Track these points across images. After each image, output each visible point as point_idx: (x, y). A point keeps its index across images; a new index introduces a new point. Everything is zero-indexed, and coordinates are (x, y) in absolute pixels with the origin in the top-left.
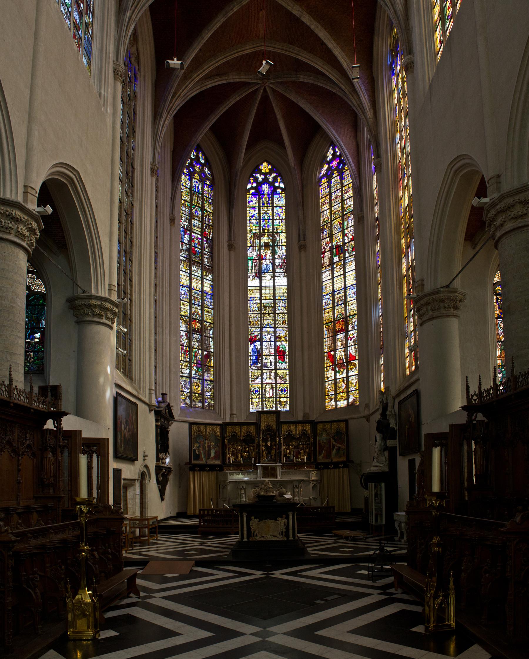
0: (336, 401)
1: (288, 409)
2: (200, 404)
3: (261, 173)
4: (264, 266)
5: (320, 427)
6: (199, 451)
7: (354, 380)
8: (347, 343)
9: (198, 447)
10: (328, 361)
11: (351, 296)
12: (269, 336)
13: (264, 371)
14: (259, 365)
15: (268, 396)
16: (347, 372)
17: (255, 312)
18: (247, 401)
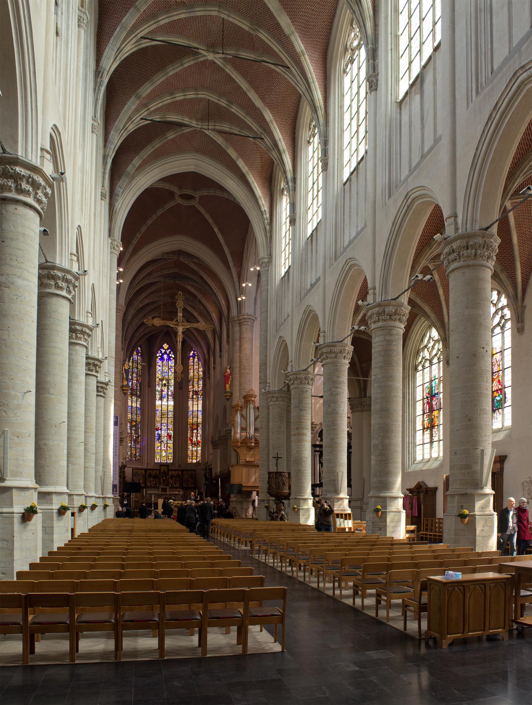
0: (192, 460)
1: (172, 462)
2: (135, 459)
3: (164, 349)
4: (163, 395)
5: (185, 472)
7: (199, 452)
8: (197, 435)
10: (189, 441)
11: (200, 416)
15: (163, 455)
16: (197, 448)
18: (154, 457)
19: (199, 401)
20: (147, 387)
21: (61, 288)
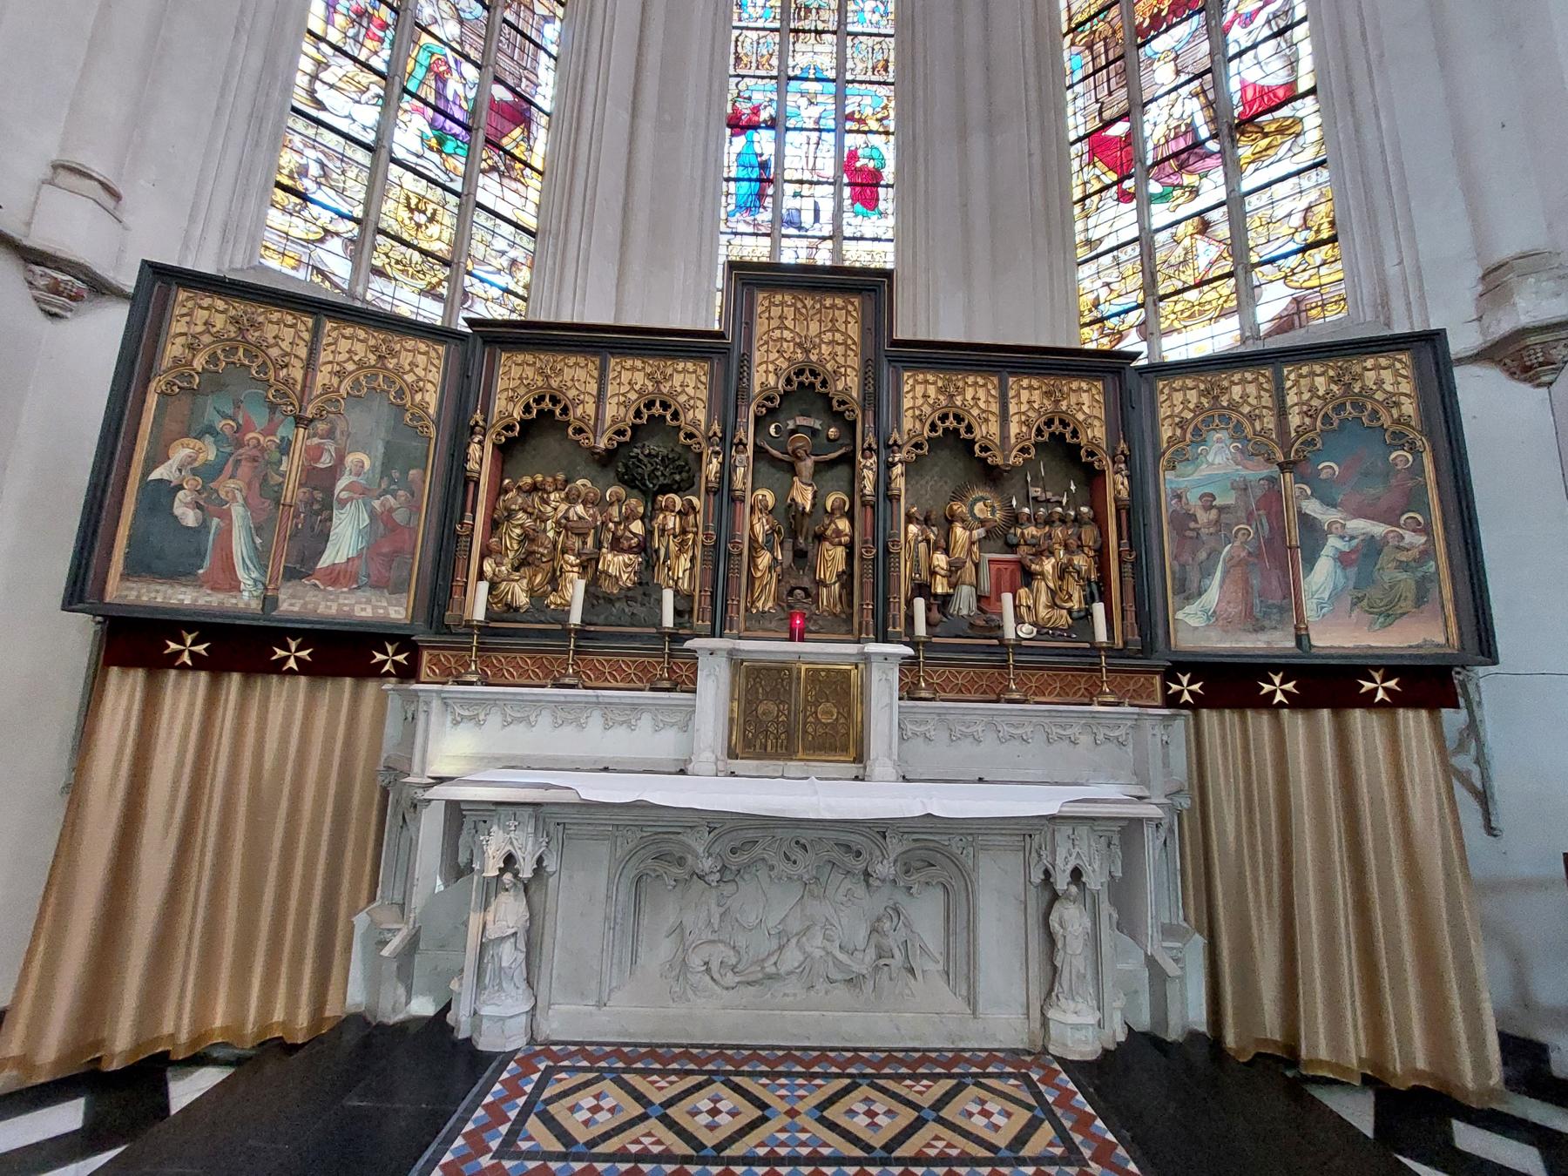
6: (209, 504)
9: (209, 473)
12: (815, 111)
13: (785, 242)
14: (765, 216)
17: (760, 24)
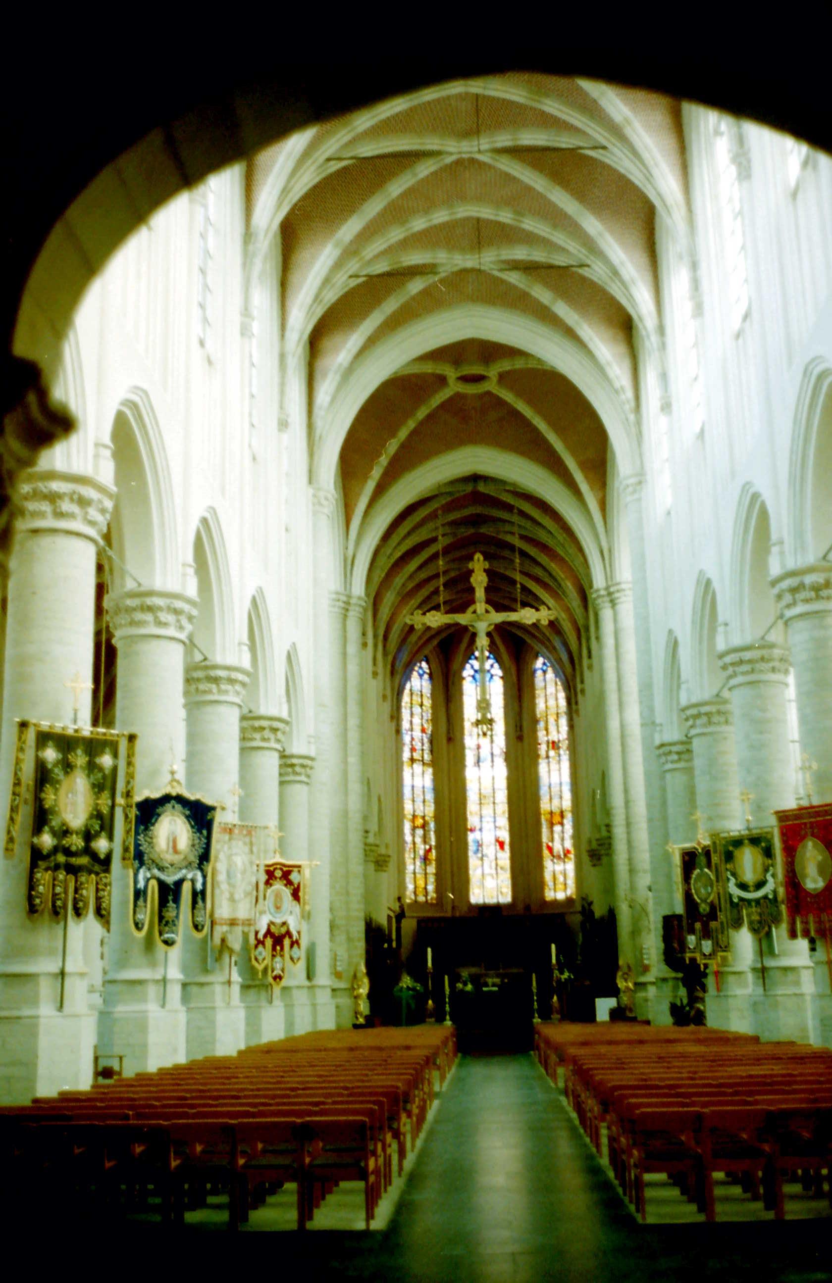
19: (562, 763)
20: (445, 741)
21: (165, 625)
